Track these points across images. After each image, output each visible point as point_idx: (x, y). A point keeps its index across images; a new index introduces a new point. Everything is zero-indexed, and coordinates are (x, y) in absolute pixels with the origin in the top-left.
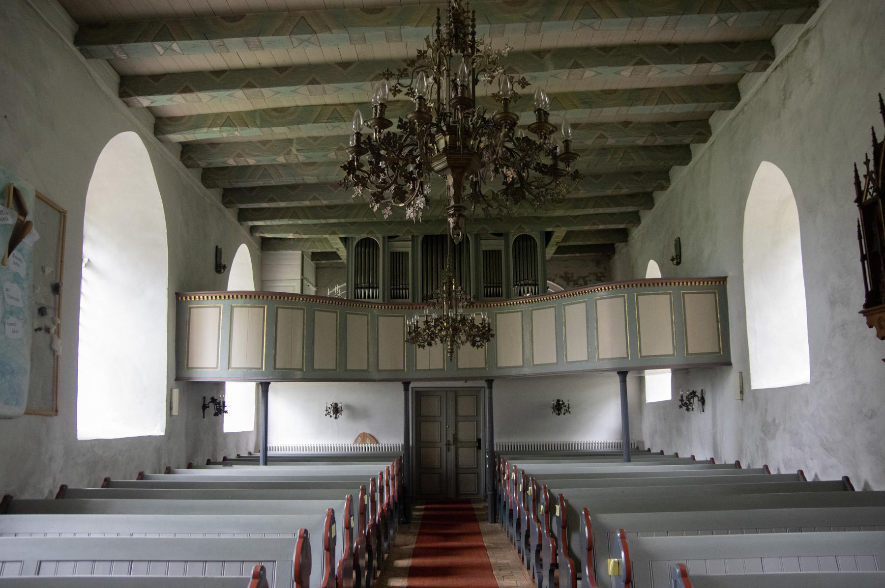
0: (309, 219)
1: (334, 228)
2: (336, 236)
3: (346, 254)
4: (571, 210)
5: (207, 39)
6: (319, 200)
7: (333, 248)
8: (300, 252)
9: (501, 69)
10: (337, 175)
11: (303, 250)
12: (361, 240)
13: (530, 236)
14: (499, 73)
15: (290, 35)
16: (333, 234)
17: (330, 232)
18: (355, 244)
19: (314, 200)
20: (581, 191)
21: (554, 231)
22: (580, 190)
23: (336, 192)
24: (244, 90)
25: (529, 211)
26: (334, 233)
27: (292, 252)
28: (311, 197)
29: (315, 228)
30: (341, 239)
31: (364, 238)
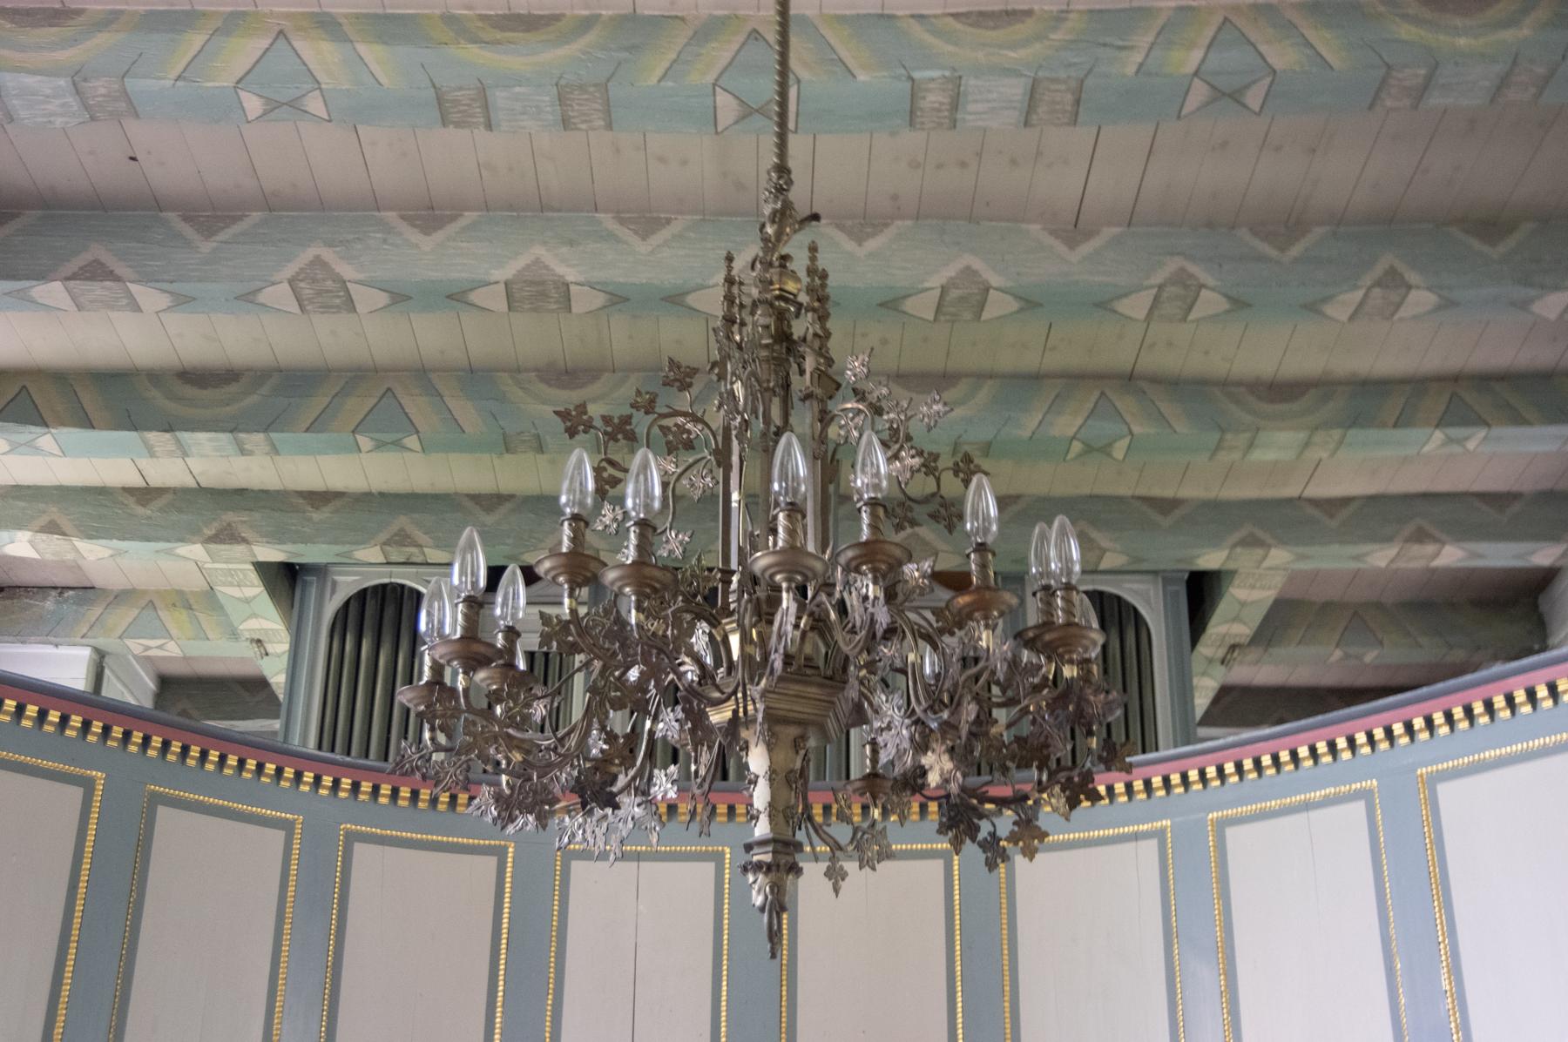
0: (90, 425)
1: (229, 516)
2: (239, 549)
3: (286, 647)
4: (1336, 433)
5: (136, 430)
6: (118, 279)
7: (234, 634)
8: (85, 653)
9: (913, 457)
10: (179, 78)
11: (101, 642)
12: (362, 595)
13: (1119, 598)
14: (904, 467)
15: (353, 432)
16: (222, 542)
17: (209, 532)
18: (332, 606)
19: (92, 278)
20: (1414, 294)
21: (1232, 573)
22: (1409, 287)
23: (206, 247)
24: (287, 654)
25: (1136, 429)
26: (228, 536)
27: (49, 650)
28: (74, 265)
29: (140, 510)
30: (262, 568)
31: (376, 588)
